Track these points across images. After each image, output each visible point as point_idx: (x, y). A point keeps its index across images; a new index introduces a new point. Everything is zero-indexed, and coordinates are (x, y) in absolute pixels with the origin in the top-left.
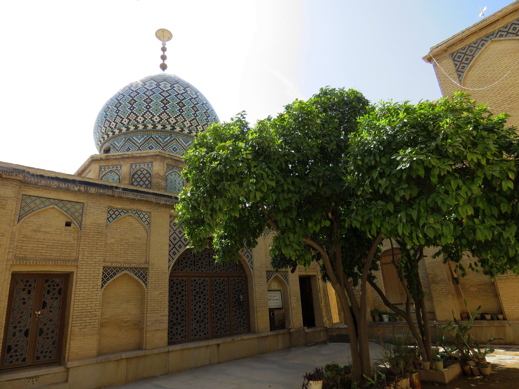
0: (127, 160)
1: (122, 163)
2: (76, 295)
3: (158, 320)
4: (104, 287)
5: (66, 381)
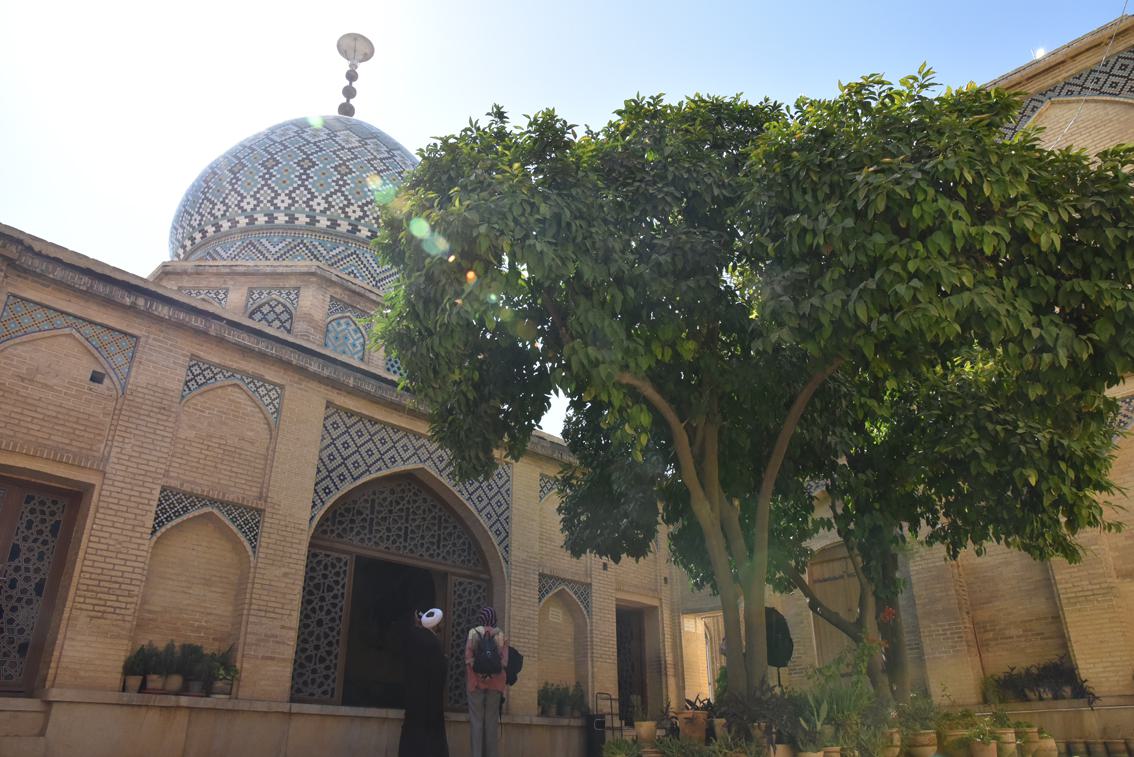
0: (243, 279)
1: (230, 284)
2: (86, 563)
3: (273, 636)
4: (158, 534)
5: (42, 733)
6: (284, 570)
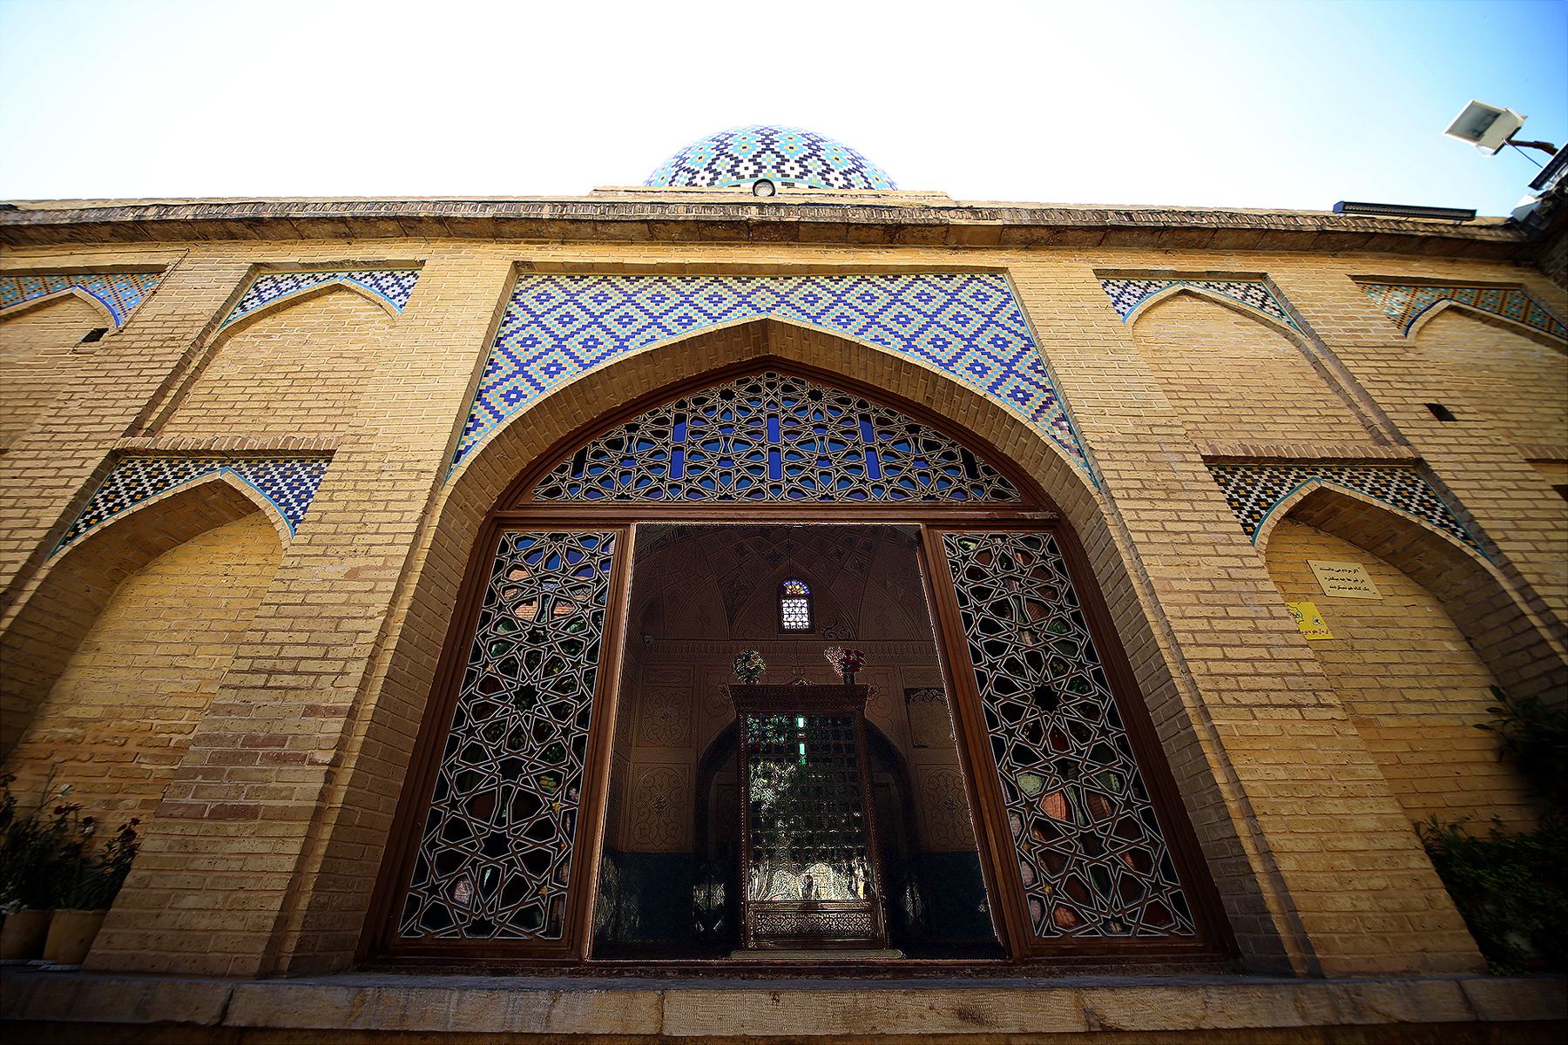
6: (351, 563)
